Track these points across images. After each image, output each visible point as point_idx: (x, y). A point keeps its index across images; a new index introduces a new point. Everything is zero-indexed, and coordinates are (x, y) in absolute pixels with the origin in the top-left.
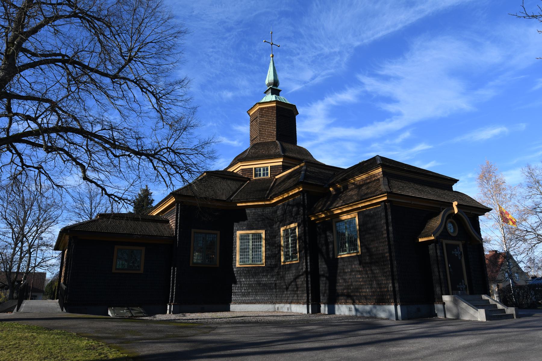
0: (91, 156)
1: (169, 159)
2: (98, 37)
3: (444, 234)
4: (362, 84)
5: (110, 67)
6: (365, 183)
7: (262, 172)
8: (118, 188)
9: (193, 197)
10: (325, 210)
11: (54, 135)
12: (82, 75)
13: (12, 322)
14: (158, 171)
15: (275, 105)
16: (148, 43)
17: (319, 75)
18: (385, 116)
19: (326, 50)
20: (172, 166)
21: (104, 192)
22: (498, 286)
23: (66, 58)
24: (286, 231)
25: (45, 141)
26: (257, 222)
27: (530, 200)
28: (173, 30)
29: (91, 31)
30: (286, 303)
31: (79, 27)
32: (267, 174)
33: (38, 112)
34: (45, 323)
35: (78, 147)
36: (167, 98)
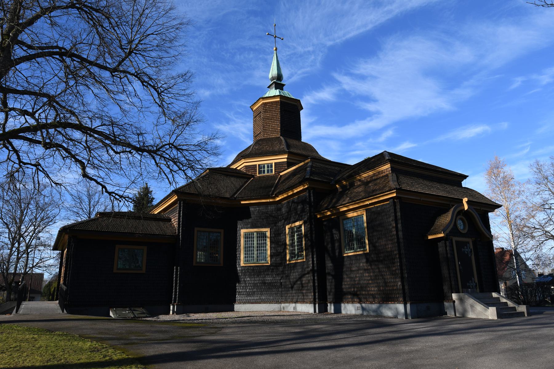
0: (90, 152)
1: (172, 156)
2: (97, 29)
3: (453, 231)
4: (339, 83)
5: (110, 61)
6: (372, 180)
7: (266, 169)
8: (119, 185)
9: (198, 195)
10: (331, 208)
11: (52, 131)
12: (81, 68)
13: (12, 324)
14: (161, 168)
15: (279, 99)
16: (149, 35)
17: (296, 73)
18: (365, 115)
19: (300, 50)
20: (175, 163)
21: (104, 189)
22: (506, 284)
23: (63, 51)
24: (291, 229)
25: (43, 137)
26: (261, 220)
27: (538, 196)
28: (174, 22)
29: (89, 23)
30: (292, 302)
31: (76, 18)
32: (272, 170)
33: (36, 107)
34: (46, 325)
35: (76, 143)
36: (169, 92)
